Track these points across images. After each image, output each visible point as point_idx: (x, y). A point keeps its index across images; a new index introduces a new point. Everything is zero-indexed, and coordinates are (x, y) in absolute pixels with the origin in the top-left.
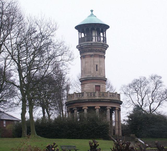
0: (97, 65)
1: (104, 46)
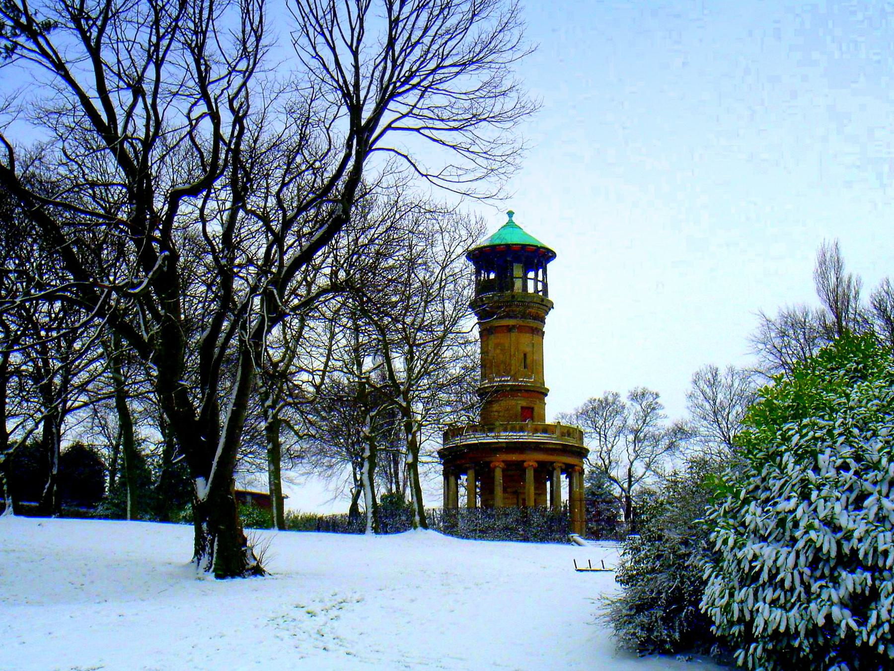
0: (525, 355)
1: (543, 305)
